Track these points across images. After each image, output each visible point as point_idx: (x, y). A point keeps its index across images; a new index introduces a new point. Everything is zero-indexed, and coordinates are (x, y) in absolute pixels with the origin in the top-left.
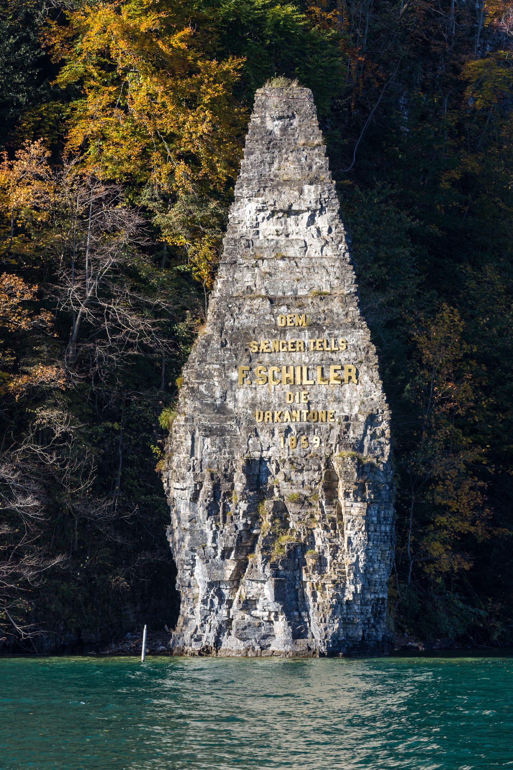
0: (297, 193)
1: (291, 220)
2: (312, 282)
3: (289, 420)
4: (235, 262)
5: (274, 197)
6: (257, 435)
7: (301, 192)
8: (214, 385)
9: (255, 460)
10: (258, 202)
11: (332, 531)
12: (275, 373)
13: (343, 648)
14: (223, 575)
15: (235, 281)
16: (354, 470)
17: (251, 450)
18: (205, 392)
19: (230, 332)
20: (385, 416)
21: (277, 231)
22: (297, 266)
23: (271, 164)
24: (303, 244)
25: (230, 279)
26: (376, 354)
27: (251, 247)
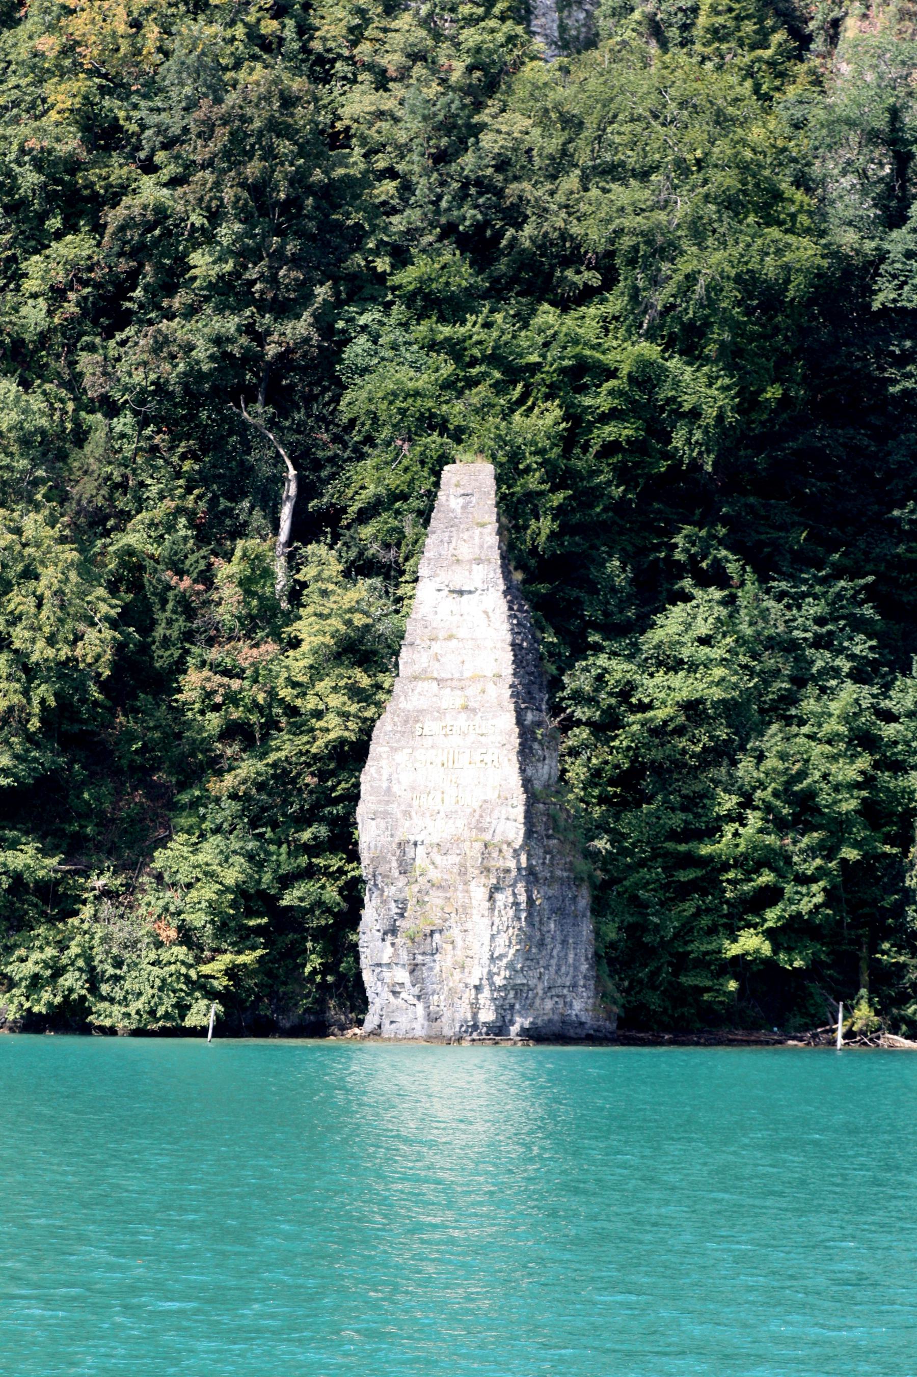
23: (449, 542)
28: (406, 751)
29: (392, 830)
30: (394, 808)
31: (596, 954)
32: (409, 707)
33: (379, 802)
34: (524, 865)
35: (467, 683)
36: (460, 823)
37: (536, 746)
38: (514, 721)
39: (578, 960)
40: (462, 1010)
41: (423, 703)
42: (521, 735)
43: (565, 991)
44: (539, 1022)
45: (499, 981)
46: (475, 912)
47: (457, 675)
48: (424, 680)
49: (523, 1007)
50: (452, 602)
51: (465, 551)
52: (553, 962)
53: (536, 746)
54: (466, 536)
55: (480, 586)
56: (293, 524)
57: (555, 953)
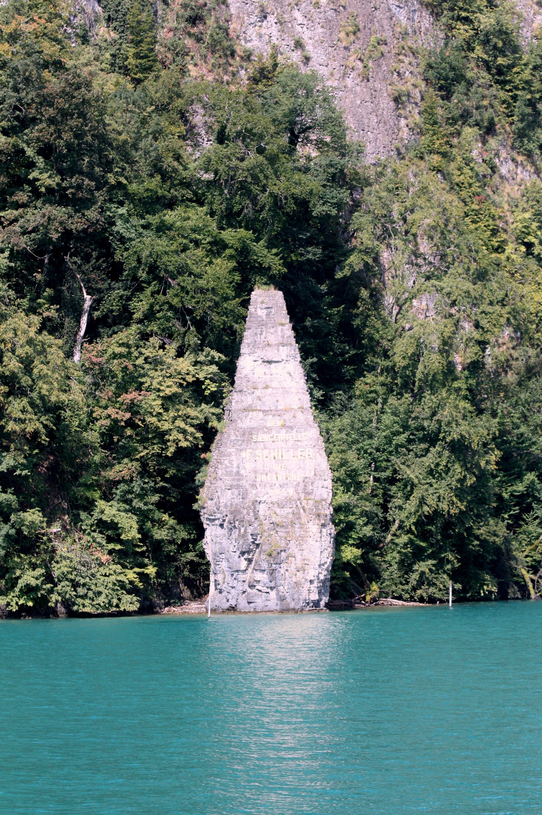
23: (261, 334)
30: (243, 483)
32: (244, 426)
33: (233, 480)
40: (304, 594)
41: (253, 424)
45: (322, 577)
48: (253, 411)
50: (265, 368)
54: (272, 330)
55: (285, 358)
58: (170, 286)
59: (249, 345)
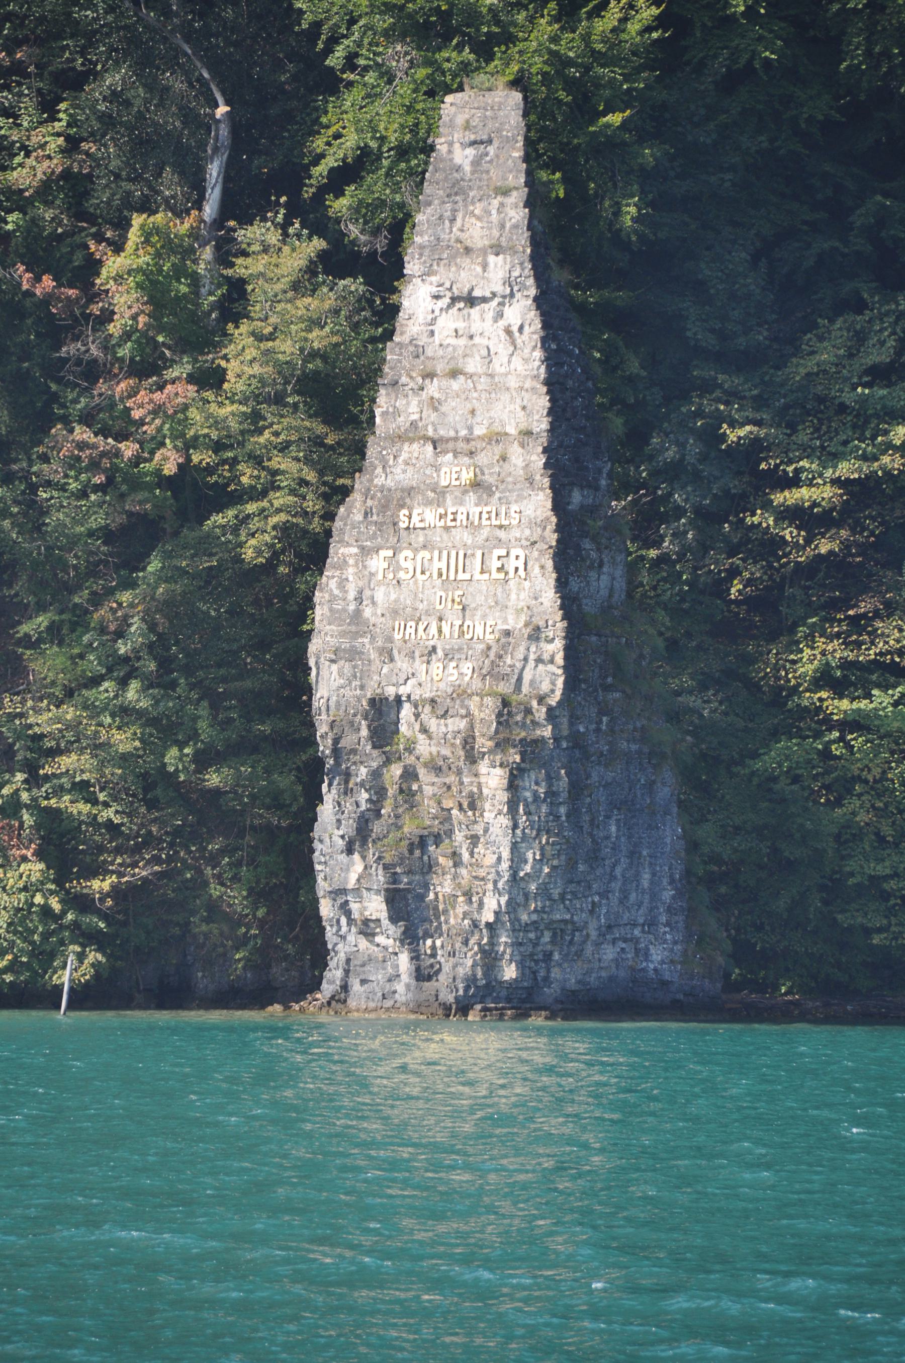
0: (479, 269)
1: (475, 312)
2: (492, 413)
3: (436, 636)
4: (397, 383)
5: (451, 275)
6: (392, 660)
7: (485, 266)
8: (347, 579)
9: (387, 699)
10: (431, 284)
11: (470, 813)
12: (425, 560)
13: (485, 998)
14: (346, 880)
15: (397, 412)
16: (494, 717)
17: (383, 684)
18: (336, 592)
19: (379, 495)
20: (557, 627)
21: (456, 331)
22: (475, 387)
23: (453, 220)
24: (484, 352)
25: (391, 410)
26: (555, 531)
27: (422, 358)
28: (384, 553)
29: (359, 676)
31: (688, 873)
32: (390, 483)
34: (565, 733)
35: (480, 445)
36: (467, 668)
37: (587, 544)
38: (549, 505)
39: (657, 880)
42: (559, 529)
43: (637, 932)
44: (592, 979)
46: (487, 806)
47: (463, 433)
48: (411, 441)
49: (565, 957)
51: (476, 233)
52: (616, 886)
53: (587, 544)
55: (499, 288)
56: (225, 192)
57: (618, 871)
58: (460, 52)
59: (422, 247)
